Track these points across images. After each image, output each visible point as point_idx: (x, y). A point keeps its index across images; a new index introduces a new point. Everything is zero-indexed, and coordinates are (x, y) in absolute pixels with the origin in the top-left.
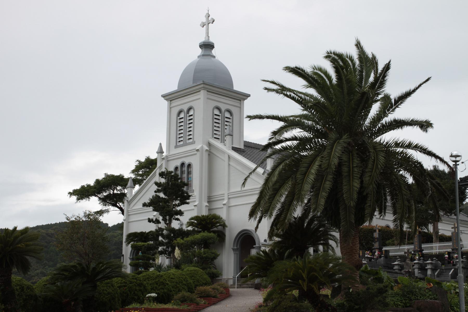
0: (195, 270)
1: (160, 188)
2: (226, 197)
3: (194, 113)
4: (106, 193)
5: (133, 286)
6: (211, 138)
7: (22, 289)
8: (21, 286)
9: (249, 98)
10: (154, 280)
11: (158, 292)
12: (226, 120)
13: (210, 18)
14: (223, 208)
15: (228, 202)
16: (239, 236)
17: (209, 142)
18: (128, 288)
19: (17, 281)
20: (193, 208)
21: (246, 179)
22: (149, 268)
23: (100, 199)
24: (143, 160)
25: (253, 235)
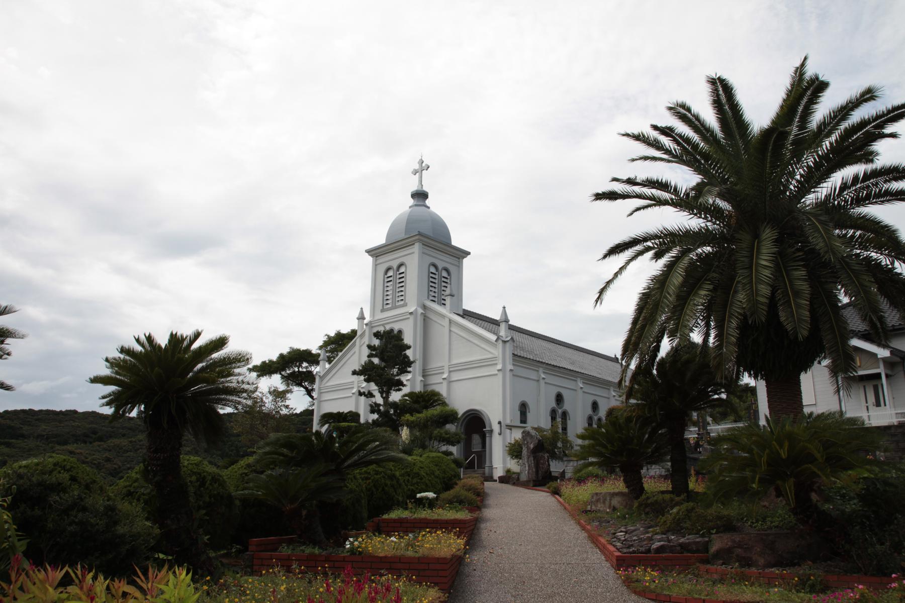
0: (439, 457)
1: (374, 353)
2: (446, 370)
4: (289, 370)
5: (380, 478)
7: (202, 481)
8: (200, 476)
9: (469, 256)
10: (403, 469)
11: (413, 487)
12: (444, 279)
13: (424, 165)
14: (442, 383)
15: (449, 376)
16: (469, 413)
18: (372, 482)
19: (191, 464)
21: (602, 292)
23: (283, 377)
24: (332, 334)
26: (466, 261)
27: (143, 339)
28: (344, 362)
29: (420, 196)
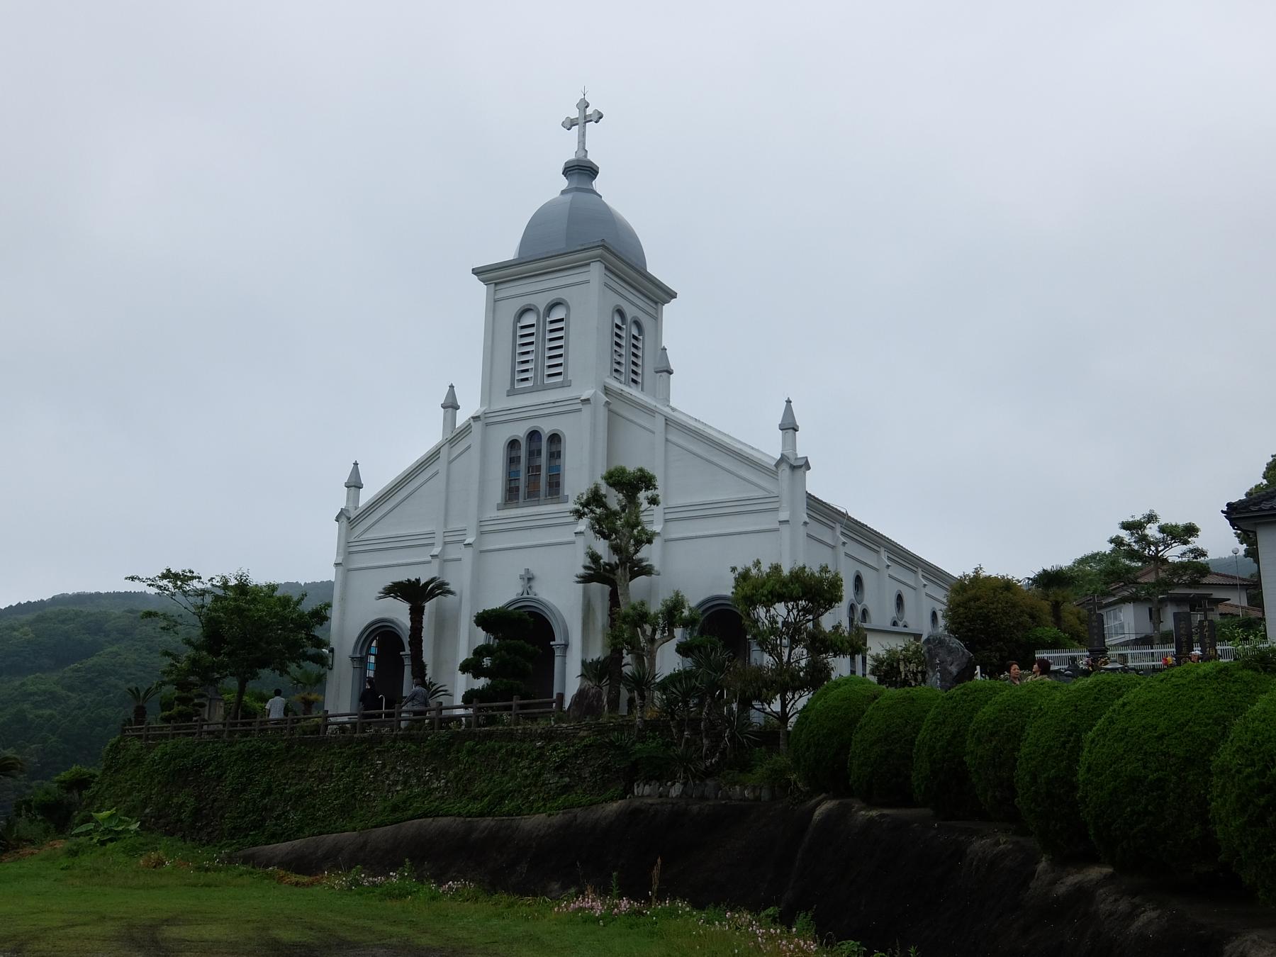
2: (439, 540)
5: (911, 750)
6: (608, 377)
13: (589, 111)
17: (606, 385)
20: (572, 538)
26: (668, 309)
28: (406, 494)
29: (581, 171)
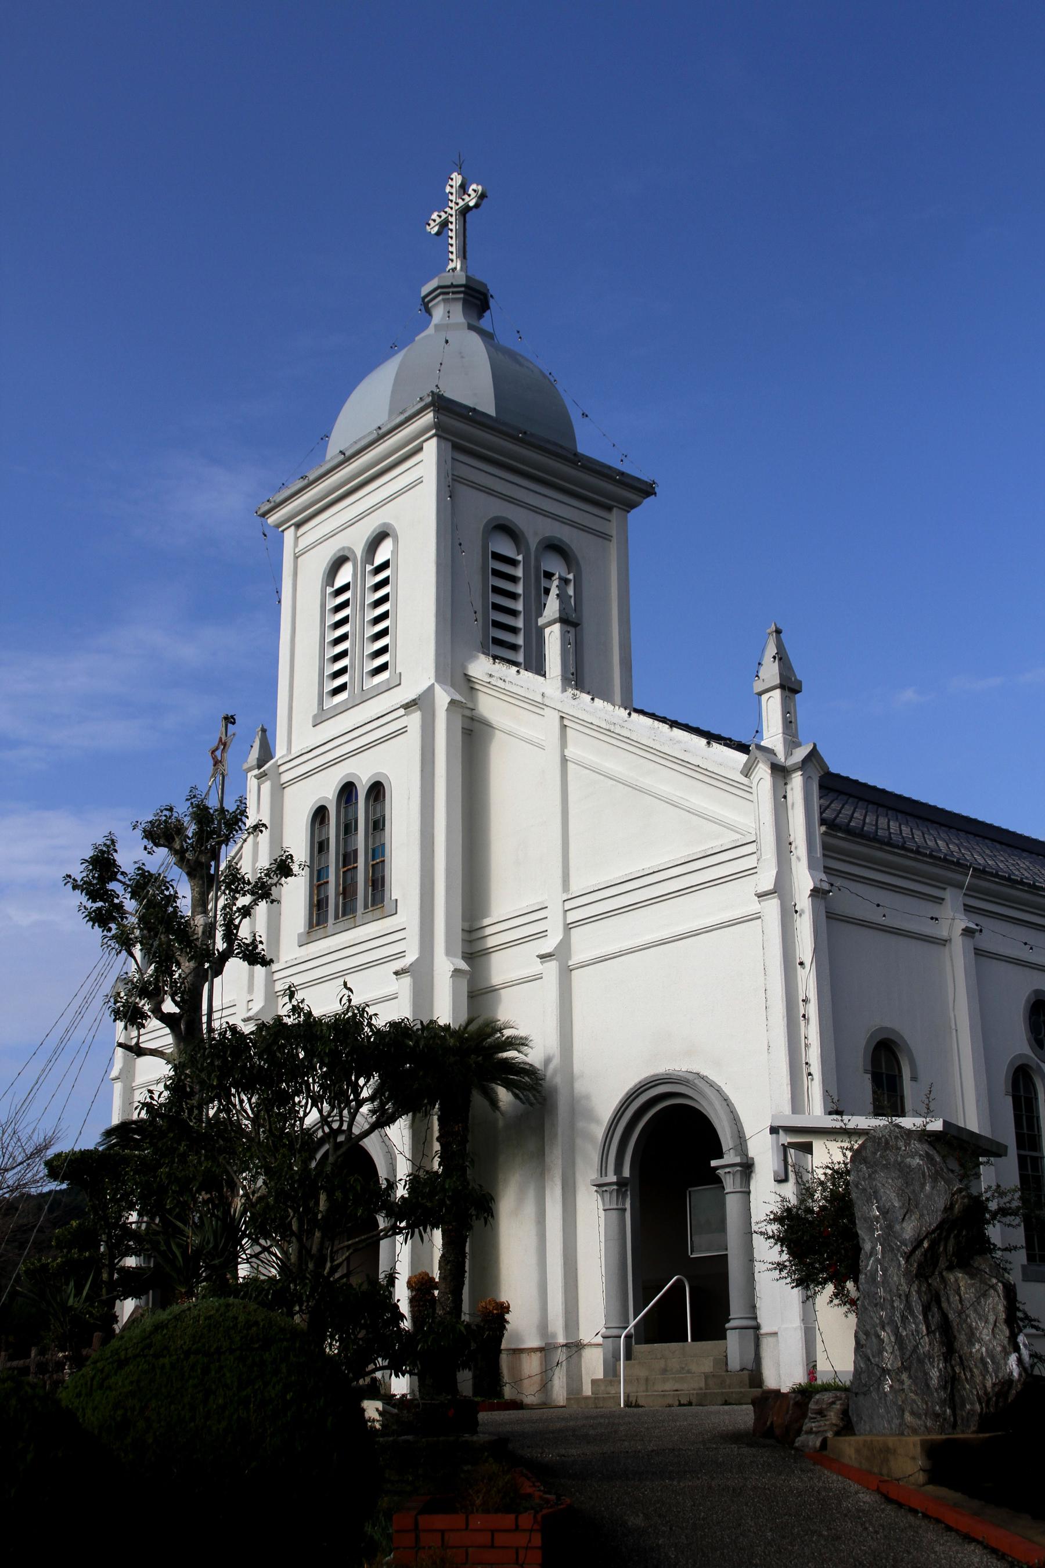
3: (395, 552)
22: (414, 1293)
25: (704, 1103)
26: (485, 199)
27: (1011, 1272)
